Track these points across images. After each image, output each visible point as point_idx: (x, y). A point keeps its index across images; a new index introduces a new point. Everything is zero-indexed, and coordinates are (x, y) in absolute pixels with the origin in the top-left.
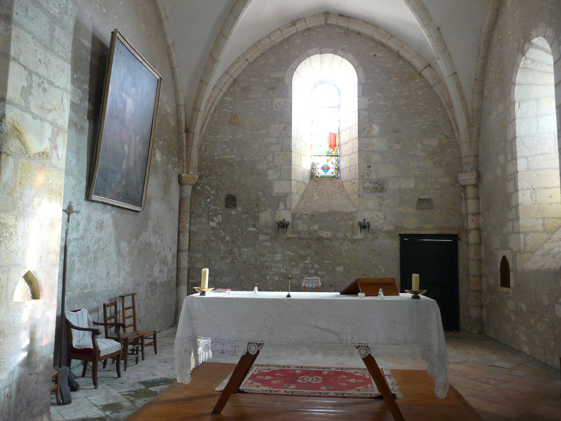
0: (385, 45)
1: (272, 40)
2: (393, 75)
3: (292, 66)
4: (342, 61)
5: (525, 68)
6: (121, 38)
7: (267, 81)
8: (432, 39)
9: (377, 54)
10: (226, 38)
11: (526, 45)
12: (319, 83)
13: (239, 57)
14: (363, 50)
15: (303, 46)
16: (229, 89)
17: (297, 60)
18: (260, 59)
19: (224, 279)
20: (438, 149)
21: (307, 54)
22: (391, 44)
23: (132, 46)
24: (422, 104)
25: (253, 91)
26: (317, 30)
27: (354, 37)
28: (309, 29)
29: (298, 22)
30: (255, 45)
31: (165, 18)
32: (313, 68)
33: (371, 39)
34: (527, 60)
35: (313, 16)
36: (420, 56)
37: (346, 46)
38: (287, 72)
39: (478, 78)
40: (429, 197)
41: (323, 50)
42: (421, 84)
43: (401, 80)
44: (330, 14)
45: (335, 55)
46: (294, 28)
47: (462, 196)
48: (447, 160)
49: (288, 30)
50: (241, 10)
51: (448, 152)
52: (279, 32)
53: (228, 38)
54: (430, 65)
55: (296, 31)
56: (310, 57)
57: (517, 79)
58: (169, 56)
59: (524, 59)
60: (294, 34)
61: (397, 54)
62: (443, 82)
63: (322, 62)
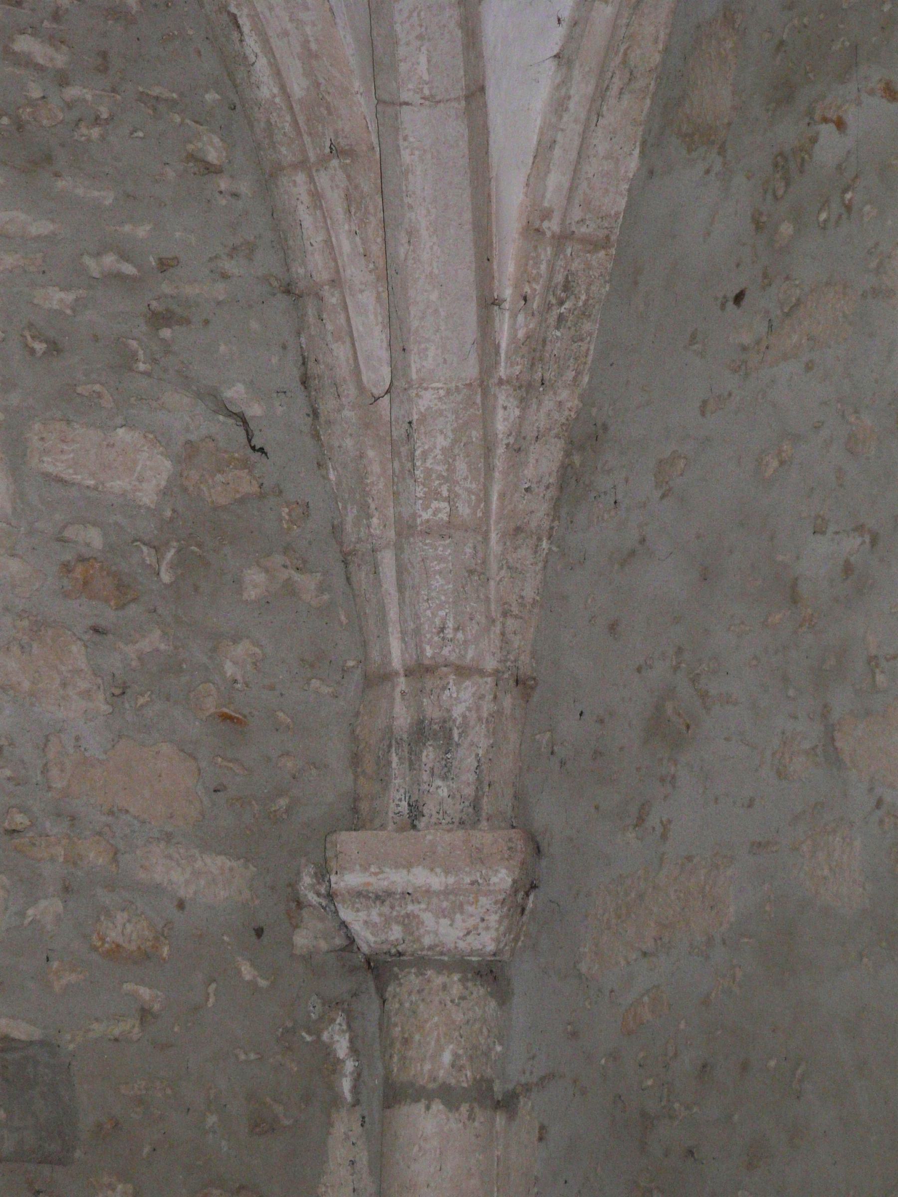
19: (449, 551)
20: (158, 549)
24: (60, 59)
40: (36, 1033)
47: (340, 1062)
48: (230, 669)
51: (251, 594)
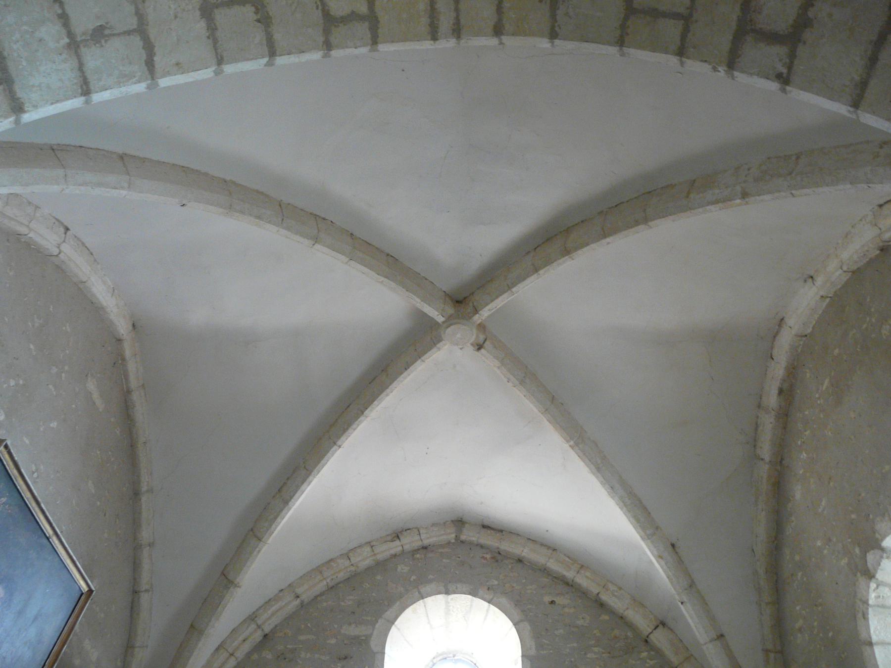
0: (571, 583)
1: (353, 562)
2: (593, 642)
3: (389, 614)
4: (487, 611)
5: (883, 606)
6: (11, 463)
7: (333, 641)
8: (666, 564)
9: (558, 600)
10: (260, 540)
11: (871, 557)
12: (441, 657)
13: (282, 590)
14: (529, 591)
15: (413, 577)
16: (249, 655)
17: (398, 603)
18: (324, 597)
21: (419, 593)
22: (583, 581)
23: (35, 491)
25: (301, 662)
26: (440, 551)
27: (510, 567)
28: (425, 548)
29: (404, 533)
30: (319, 570)
31: (147, 491)
32: (429, 623)
33: (545, 571)
34: (881, 588)
35: (433, 525)
36: (642, 605)
37: (496, 583)
38: (377, 626)
39: (770, 646)
41: (451, 587)
42: (652, 662)
43: (609, 653)
44: (466, 523)
45: (474, 598)
46: (397, 543)
49: (384, 547)
50: (298, 488)
52: (367, 549)
53: (263, 540)
54: (663, 624)
55: (401, 548)
56: (425, 599)
57: (872, 632)
58: (136, 565)
59: (873, 585)
60: (395, 556)
61: (596, 600)
62: (696, 659)
63: (448, 612)
